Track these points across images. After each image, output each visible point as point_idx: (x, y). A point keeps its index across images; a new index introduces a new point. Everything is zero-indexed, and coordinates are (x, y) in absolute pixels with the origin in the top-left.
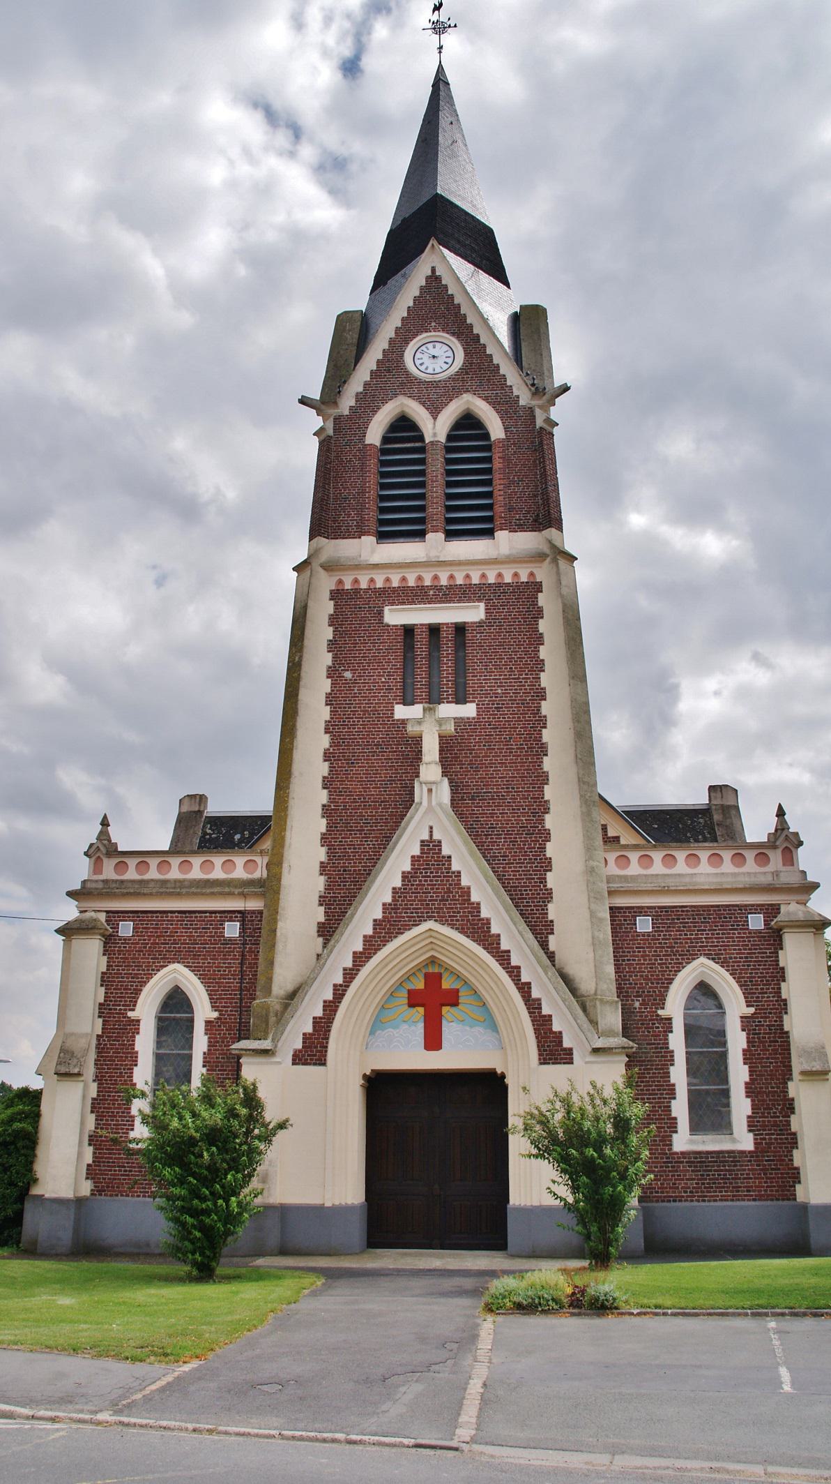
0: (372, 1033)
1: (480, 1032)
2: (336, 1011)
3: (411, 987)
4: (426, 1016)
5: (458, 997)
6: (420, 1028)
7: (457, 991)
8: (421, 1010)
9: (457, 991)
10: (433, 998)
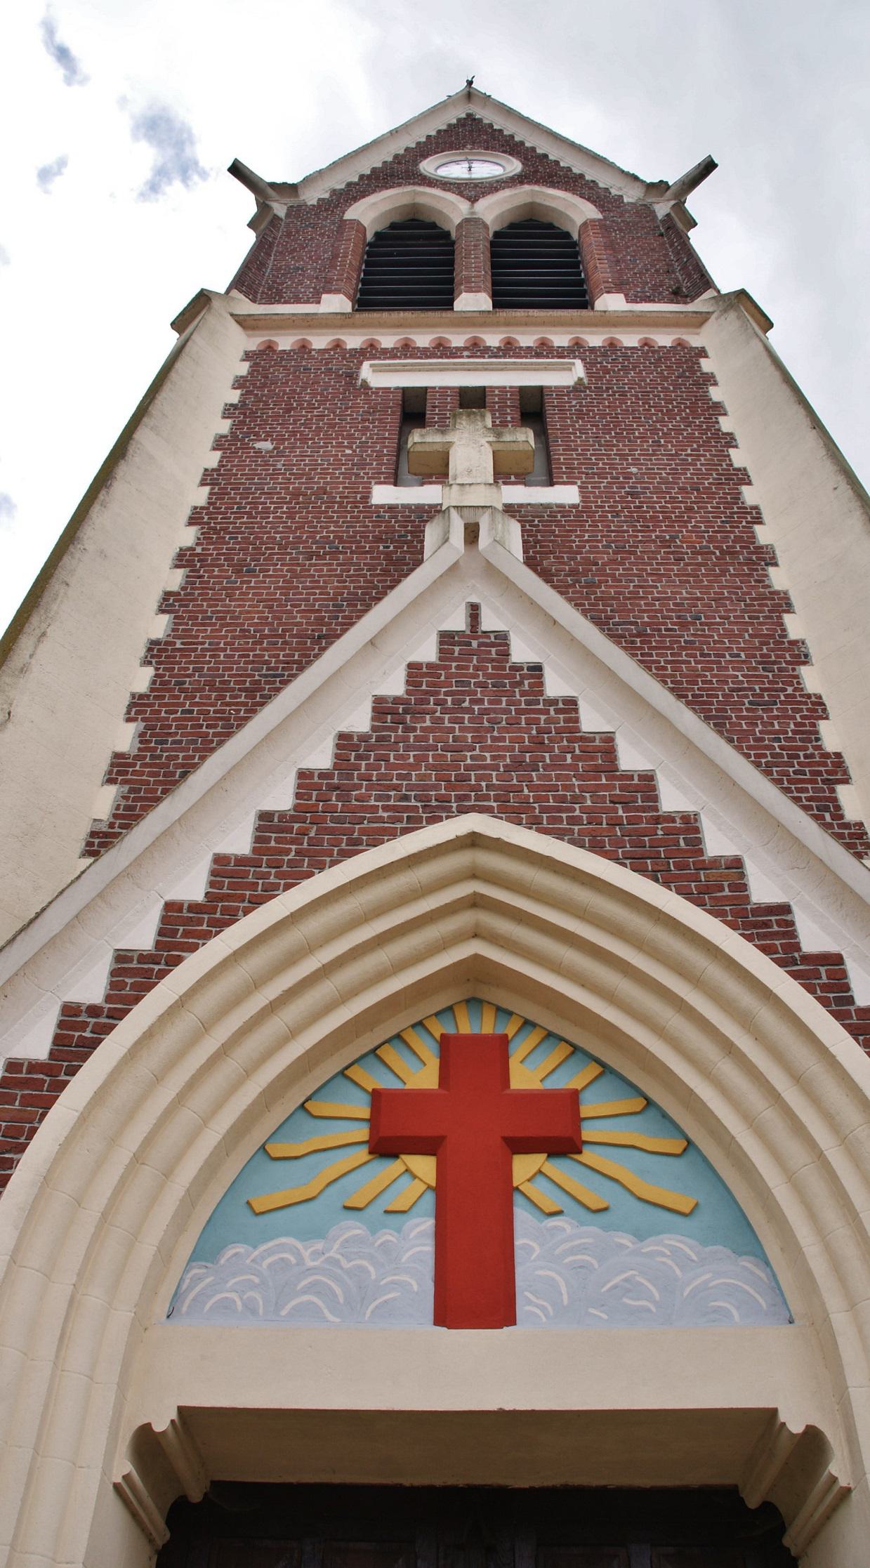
0: (205, 1252)
1: (682, 1257)
2: (48, 1104)
3: (387, 1082)
4: (441, 1190)
5: (577, 1120)
6: (416, 1240)
7: (573, 1097)
8: (425, 1166)
9: (573, 1097)
10: (473, 1128)
